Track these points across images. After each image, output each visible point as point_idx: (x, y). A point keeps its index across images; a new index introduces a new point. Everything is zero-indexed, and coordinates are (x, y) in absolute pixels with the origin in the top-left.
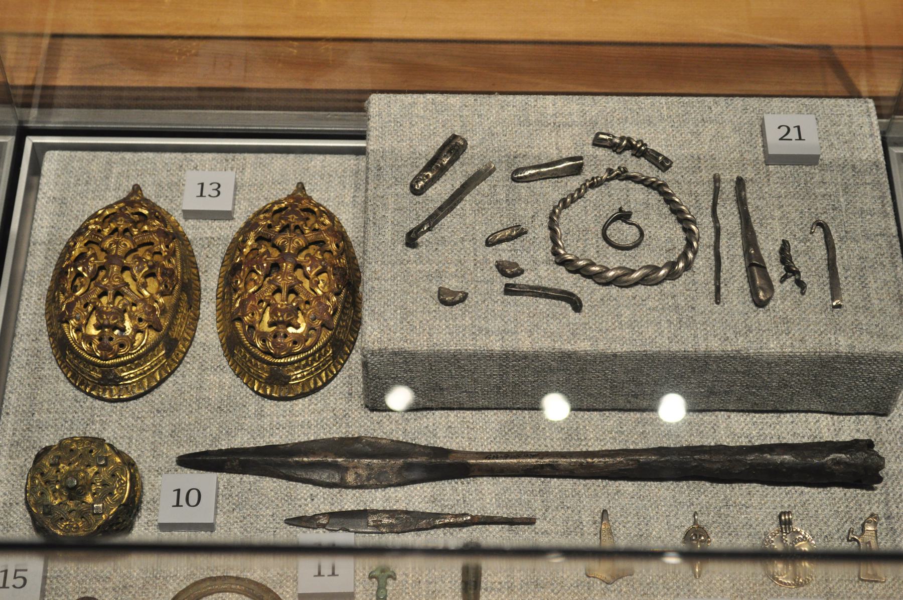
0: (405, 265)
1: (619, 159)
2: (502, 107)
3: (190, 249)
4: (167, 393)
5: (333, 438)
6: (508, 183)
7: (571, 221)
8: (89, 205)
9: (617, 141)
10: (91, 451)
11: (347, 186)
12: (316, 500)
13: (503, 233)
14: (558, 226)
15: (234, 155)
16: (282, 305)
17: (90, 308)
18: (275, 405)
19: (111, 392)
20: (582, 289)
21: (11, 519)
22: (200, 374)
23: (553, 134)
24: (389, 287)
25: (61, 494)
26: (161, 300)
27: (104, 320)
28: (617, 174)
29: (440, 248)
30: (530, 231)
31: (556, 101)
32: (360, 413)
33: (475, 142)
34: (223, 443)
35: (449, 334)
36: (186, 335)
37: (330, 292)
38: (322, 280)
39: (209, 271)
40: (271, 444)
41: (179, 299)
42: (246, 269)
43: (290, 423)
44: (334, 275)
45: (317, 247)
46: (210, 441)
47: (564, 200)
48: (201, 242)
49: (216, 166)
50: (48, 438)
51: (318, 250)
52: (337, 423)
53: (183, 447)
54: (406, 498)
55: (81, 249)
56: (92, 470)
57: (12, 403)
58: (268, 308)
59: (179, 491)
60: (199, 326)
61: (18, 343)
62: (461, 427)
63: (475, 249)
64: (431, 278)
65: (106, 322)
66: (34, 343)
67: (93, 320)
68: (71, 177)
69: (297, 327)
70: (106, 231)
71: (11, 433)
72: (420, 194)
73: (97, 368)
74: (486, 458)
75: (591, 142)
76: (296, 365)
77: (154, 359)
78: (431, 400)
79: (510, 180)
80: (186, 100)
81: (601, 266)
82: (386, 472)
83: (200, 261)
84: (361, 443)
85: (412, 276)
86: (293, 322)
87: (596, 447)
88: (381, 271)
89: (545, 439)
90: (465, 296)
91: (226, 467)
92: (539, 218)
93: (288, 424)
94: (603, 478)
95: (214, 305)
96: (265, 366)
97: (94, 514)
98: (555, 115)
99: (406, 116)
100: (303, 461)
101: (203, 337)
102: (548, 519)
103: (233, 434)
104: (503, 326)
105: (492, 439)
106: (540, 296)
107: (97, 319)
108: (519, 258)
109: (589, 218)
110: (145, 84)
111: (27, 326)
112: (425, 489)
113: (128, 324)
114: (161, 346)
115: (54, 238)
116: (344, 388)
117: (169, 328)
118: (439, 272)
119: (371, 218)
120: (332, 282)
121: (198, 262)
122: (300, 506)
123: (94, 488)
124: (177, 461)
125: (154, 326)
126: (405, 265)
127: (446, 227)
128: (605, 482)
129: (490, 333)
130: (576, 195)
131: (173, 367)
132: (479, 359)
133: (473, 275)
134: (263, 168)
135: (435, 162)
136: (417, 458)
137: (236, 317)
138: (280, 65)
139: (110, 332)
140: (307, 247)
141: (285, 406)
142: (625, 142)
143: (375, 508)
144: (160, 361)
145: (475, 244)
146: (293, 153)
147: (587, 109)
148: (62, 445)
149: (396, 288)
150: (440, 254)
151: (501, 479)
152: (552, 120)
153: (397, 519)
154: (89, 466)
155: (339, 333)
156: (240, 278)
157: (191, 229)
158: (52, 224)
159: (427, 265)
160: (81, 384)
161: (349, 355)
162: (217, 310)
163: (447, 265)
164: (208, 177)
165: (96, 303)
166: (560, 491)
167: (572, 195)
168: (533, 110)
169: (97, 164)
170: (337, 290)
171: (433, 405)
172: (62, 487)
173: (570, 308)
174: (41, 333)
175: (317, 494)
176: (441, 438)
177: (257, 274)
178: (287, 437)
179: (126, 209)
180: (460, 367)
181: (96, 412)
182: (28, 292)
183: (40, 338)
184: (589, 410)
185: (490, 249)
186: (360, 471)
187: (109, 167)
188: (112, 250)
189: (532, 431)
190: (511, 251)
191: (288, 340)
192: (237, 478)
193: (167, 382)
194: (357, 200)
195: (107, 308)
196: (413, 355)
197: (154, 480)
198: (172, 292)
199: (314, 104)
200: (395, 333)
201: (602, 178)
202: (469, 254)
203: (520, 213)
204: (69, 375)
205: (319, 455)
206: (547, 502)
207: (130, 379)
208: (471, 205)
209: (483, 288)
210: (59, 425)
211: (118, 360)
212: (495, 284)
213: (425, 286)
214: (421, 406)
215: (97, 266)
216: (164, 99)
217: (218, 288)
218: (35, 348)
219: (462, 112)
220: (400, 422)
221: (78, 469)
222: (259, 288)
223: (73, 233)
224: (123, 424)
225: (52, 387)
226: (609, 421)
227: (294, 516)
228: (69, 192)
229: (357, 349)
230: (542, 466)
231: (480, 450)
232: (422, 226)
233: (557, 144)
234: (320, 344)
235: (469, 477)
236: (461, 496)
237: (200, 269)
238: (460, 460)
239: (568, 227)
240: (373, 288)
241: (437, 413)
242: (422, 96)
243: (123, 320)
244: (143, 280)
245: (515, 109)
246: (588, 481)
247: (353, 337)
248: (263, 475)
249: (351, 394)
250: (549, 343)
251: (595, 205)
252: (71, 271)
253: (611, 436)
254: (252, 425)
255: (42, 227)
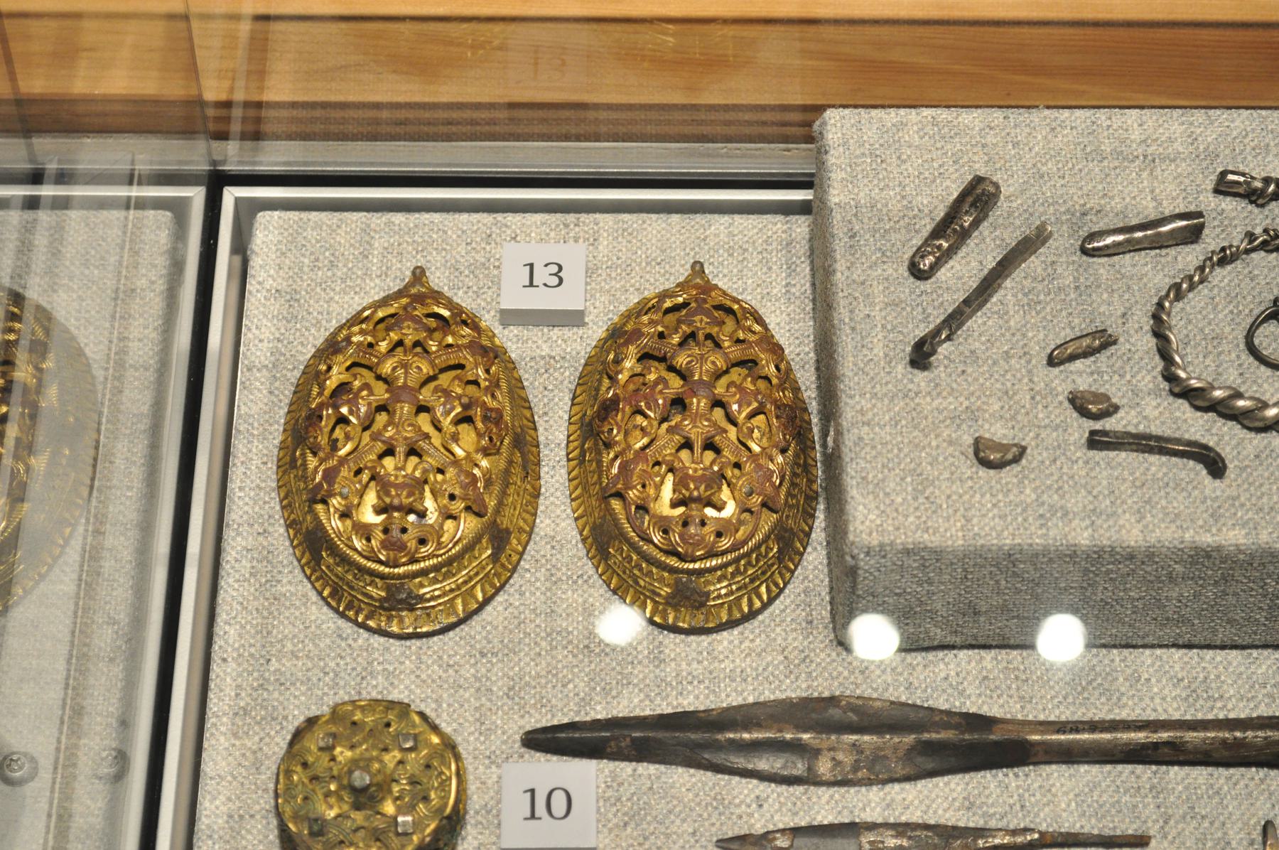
0: (912, 399)
1: (1261, 217)
2: (1053, 129)
3: (516, 375)
4: (495, 623)
5: (787, 698)
6: (1075, 258)
7: (1190, 322)
8: (337, 303)
9: (1258, 184)
10: (388, 725)
11: (775, 267)
12: (766, 806)
13: (1077, 343)
14: (1170, 329)
15: (577, 215)
16: (695, 470)
17: (365, 476)
18: (683, 641)
19: (401, 621)
20: (1221, 438)
21: (244, 842)
22: (549, 589)
23: (1145, 175)
24: (888, 438)
25: (340, 799)
26: (484, 463)
27: (392, 497)
28: (1265, 243)
29: (970, 370)
30: (1121, 340)
31: (1144, 118)
32: (829, 655)
33: (1012, 189)
34: (598, 708)
35: (1000, 517)
36: (521, 523)
37: (773, 446)
38: (758, 427)
39: (550, 415)
40: (680, 710)
41: (510, 462)
42: (627, 408)
43: (711, 673)
44: (777, 417)
45: (744, 371)
46: (576, 704)
47: (1177, 287)
48: (533, 364)
49: (548, 235)
50: (296, 702)
51: (747, 376)
52: (791, 672)
53: (531, 716)
54: (921, 802)
55: (341, 376)
56: (391, 758)
57: (231, 641)
58: (373, 484)
59: (532, 791)
60: (541, 508)
61: (234, 539)
62: (1006, 679)
63: (1030, 372)
64: (958, 421)
65: (396, 502)
66: (261, 539)
67: (371, 498)
68: (303, 255)
69: (719, 509)
70: (383, 346)
71: (233, 694)
72: (927, 279)
73: (377, 580)
74: (1058, 732)
75: (1210, 186)
76: (719, 573)
77: (474, 564)
78: (956, 632)
79: (1079, 253)
80: (488, 124)
81: (1251, 398)
82: (885, 757)
83: (534, 396)
84: (838, 706)
85: (926, 418)
86: (714, 499)
87: (1241, 711)
88: (871, 409)
89: (1152, 699)
90: (1023, 450)
91: (609, 750)
92: (1135, 318)
93: (707, 675)
94: (1259, 764)
95: (564, 471)
96: (666, 574)
97: (398, 834)
98: (1145, 141)
99: (890, 146)
100: (742, 739)
101: (548, 525)
102: (1170, 837)
103: (614, 693)
104: (1091, 502)
105: (1060, 699)
106: (1151, 450)
107: (379, 497)
108: (1107, 387)
109: (1220, 316)
110: (417, 98)
111: (246, 508)
112: (953, 786)
113: (429, 503)
114: (484, 541)
115: (282, 358)
116: (798, 612)
117: (497, 511)
118: (972, 412)
119: (847, 320)
120: (774, 429)
121: (531, 397)
122: (740, 817)
123: (396, 789)
124: (522, 740)
125: (475, 509)
126: (912, 399)
127: (976, 334)
128: (1263, 772)
129: (1071, 516)
130: (1196, 278)
131: (503, 578)
132: (1051, 560)
133: (1031, 415)
134: (629, 238)
135: (952, 223)
136: (938, 732)
137: (613, 491)
138: (646, 65)
139: (402, 518)
140: (726, 372)
141: (699, 644)
142: (1272, 187)
143: (869, 820)
144: (484, 568)
145: (1029, 362)
146: (677, 212)
147: (1198, 131)
148: (336, 714)
149: (899, 439)
150: (970, 379)
151: (1083, 768)
152: (1140, 151)
153: (910, 838)
154: (386, 750)
155: (788, 517)
156: (617, 424)
157: (511, 340)
158: (277, 335)
159: (951, 399)
160: (349, 606)
161: (802, 554)
162: (570, 480)
163: (984, 399)
164: (541, 254)
165: (375, 467)
166: (1186, 788)
167: (1191, 277)
168: (1106, 133)
169: (346, 233)
170: (783, 444)
171: (958, 640)
172: (341, 787)
173: (1204, 472)
174: (272, 521)
175: (768, 797)
176: (973, 699)
177: (646, 416)
178: (707, 697)
179: (415, 309)
180: (1015, 574)
181: (376, 655)
182: (245, 451)
183: (271, 529)
184: (1223, 647)
185: (1056, 371)
186: (840, 756)
187: (367, 238)
188: (397, 378)
189: (1128, 684)
190: (1092, 373)
191: (707, 529)
192: (625, 768)
193: (494, 603)
194: (793, 290)
195: (396, 477)
196: (938, 553)
197: (484, 773)
198: (499, 450)
199: (705, 130)
200: (906, 516)
201: (1238, 247)
202: (1020, 380)
203: (1102, 310)
204: (326, 593)
205: (768, 728)
206: (1166, 807)
207: (433, 598)
208: (1015, 296)
209: (1051, 437)
210: (314, 679)
211: (415, 567)
212: (1070, 430)
213: (950, 436)
214: (936, 643)
215: (374, 405)
216: (449, 123)
217: (568, 442)
218: (264, 547)
219: (984, 138)
220: (900, 670)
221: (367, 755)
222: (652, 441)
223: (313, 350)
224: (424, 676)
225: (297, 613)
226: (1260, 666)
227: (730, 835)
228: (302, 280)
229: (815, 544)
230: (1156, 746)
231: (1042, 717)
232: (937, 332)
233: (1152, 191)
234: (759, 536)
235: (1028, 764)
236: (1016, 797)
237: (535, 410)
238: (1013, 736)
239: (1185, 332)
240: (860, 439)
241: (963, 654)
242: (913, 111)
243: (422, 498)
244: (453, 429)
245: (1075, 132)
246: (1232, 771)
247: (807, 524)
248: (671, 764)
249: (811, 622)
250: (1174, 532)
251: (1228, 295)
252: (328, 415)
253: (1265, 691)
254: (645, 678)
255: (261, 341)
